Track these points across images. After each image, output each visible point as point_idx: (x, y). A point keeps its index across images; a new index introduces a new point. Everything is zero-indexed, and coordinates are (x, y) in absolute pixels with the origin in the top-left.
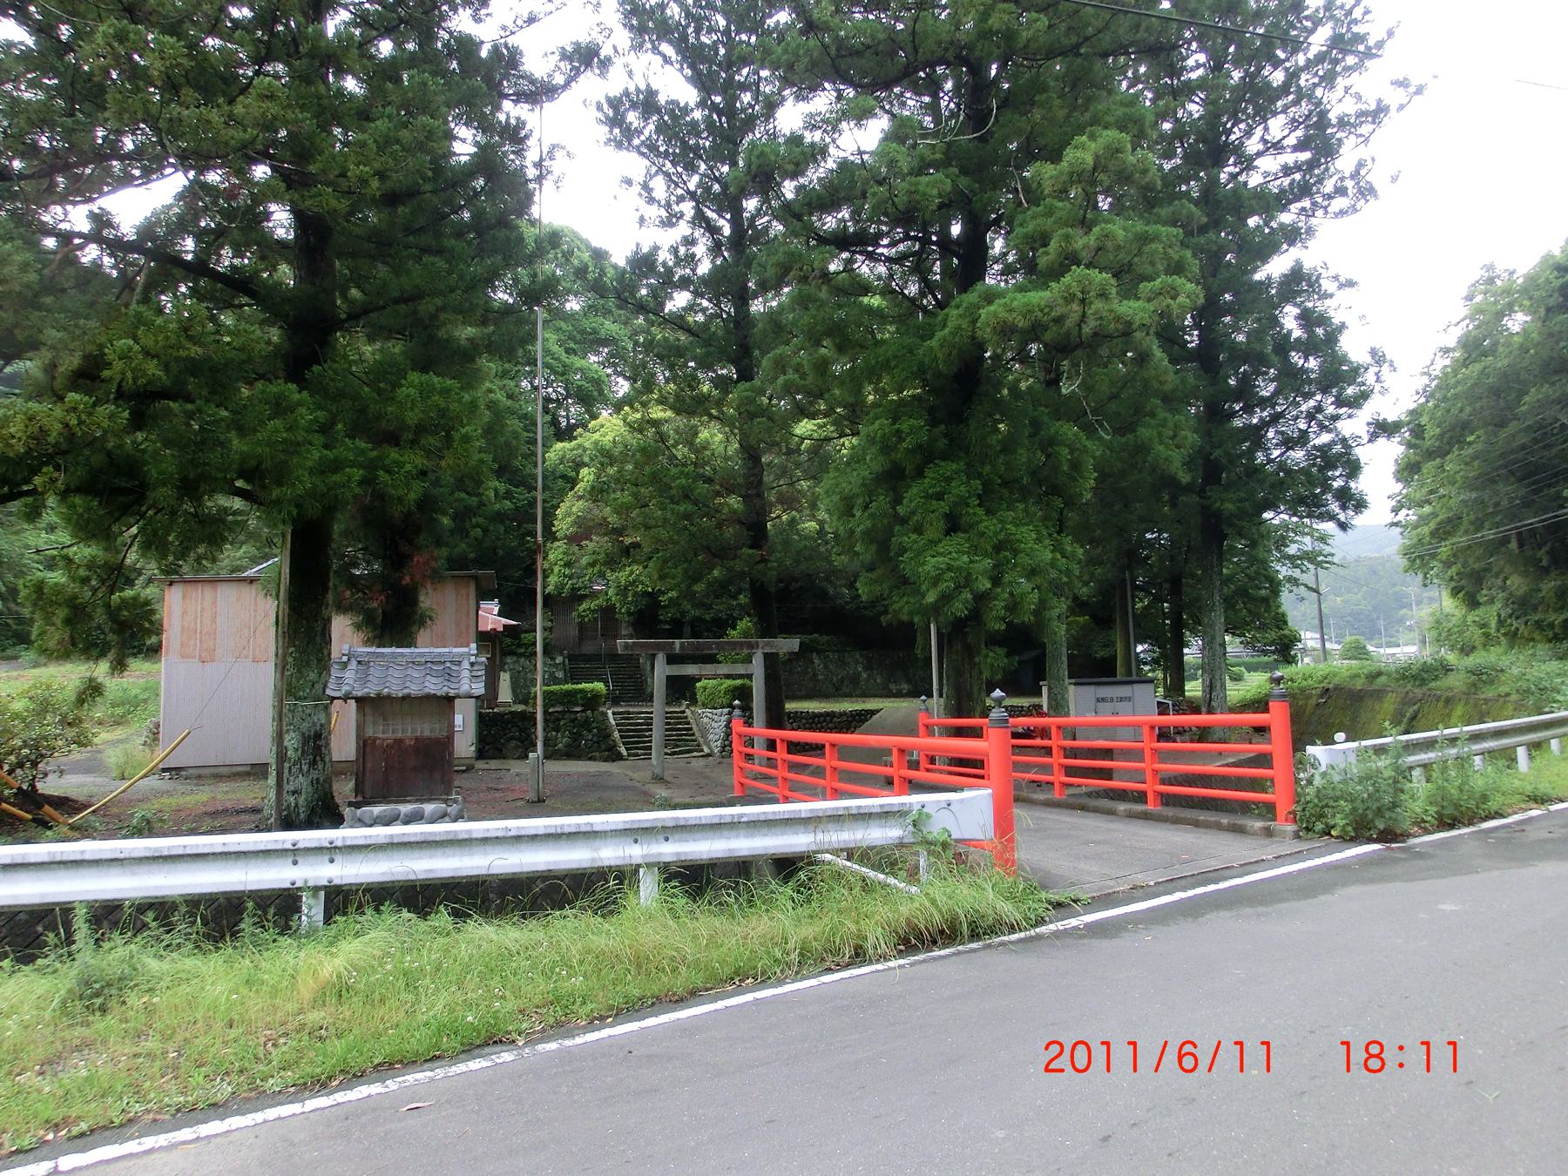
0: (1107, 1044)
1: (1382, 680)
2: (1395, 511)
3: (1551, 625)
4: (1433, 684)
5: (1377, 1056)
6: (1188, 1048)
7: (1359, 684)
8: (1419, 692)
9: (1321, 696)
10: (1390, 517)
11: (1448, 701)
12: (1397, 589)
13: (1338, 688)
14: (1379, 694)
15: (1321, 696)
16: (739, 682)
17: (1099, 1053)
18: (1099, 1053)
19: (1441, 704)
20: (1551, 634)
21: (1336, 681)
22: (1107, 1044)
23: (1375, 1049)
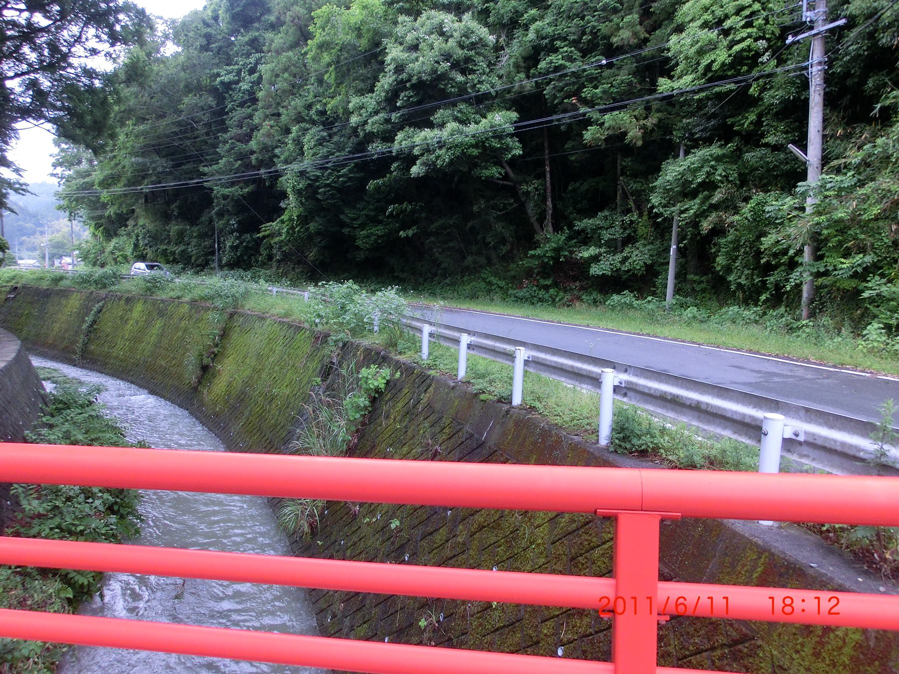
0: (635, 598)
1: (63, 283)
2: (55, 166)
3: (173, 253)
4: (112, 288)
5: (790, 605)
6: (681, 600)
7: (45, 285)
8: (103, 293)
9: (10, 293)
10: (51, 170)
11: (128, 300)
12: (21, 223)
13: (24, 287)
14: (65, 293)
15: (10, 293)
16: (781, 380)
17: (630, 604)
18: (630, 604)
19: (122, 302)
20: (171, 258)
21: (23, 281)
22: (635, 598)
23: (788, 601)
